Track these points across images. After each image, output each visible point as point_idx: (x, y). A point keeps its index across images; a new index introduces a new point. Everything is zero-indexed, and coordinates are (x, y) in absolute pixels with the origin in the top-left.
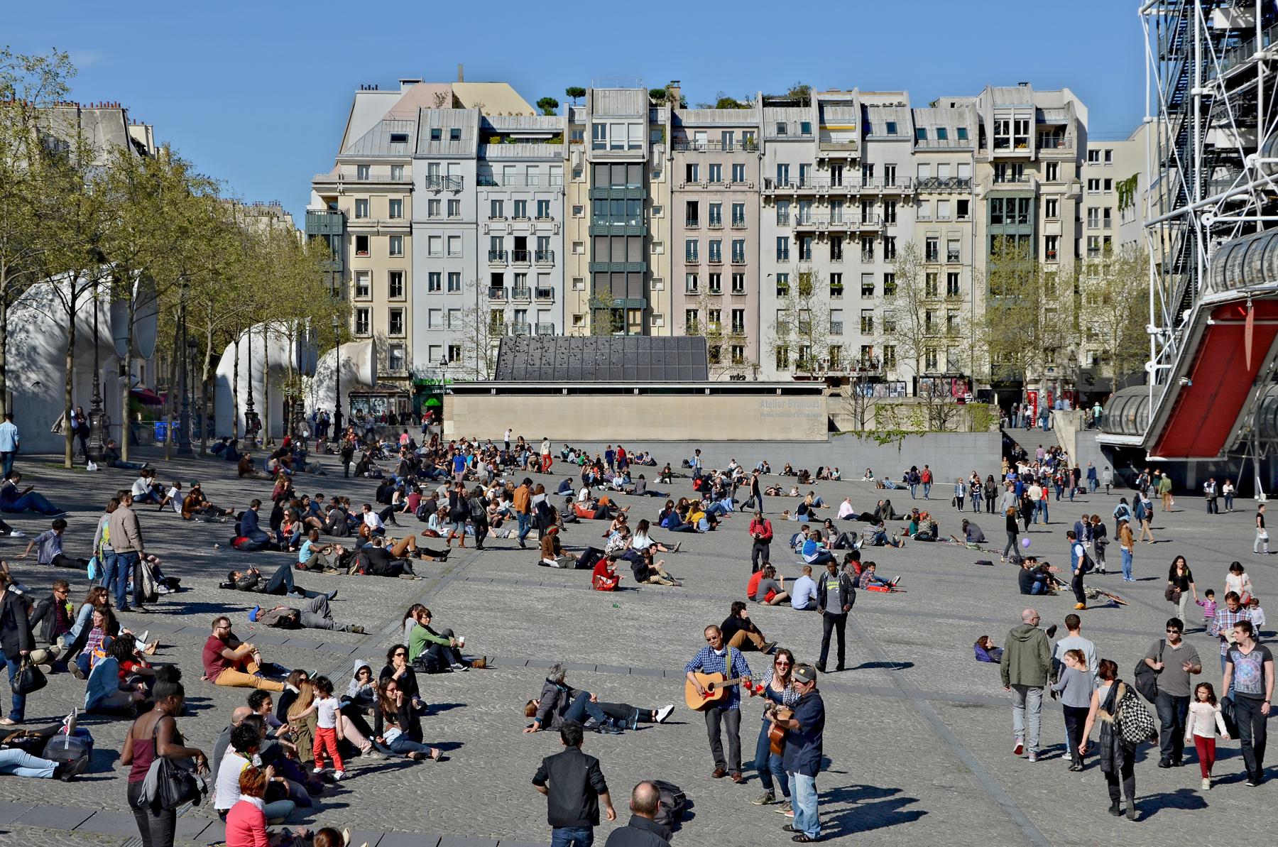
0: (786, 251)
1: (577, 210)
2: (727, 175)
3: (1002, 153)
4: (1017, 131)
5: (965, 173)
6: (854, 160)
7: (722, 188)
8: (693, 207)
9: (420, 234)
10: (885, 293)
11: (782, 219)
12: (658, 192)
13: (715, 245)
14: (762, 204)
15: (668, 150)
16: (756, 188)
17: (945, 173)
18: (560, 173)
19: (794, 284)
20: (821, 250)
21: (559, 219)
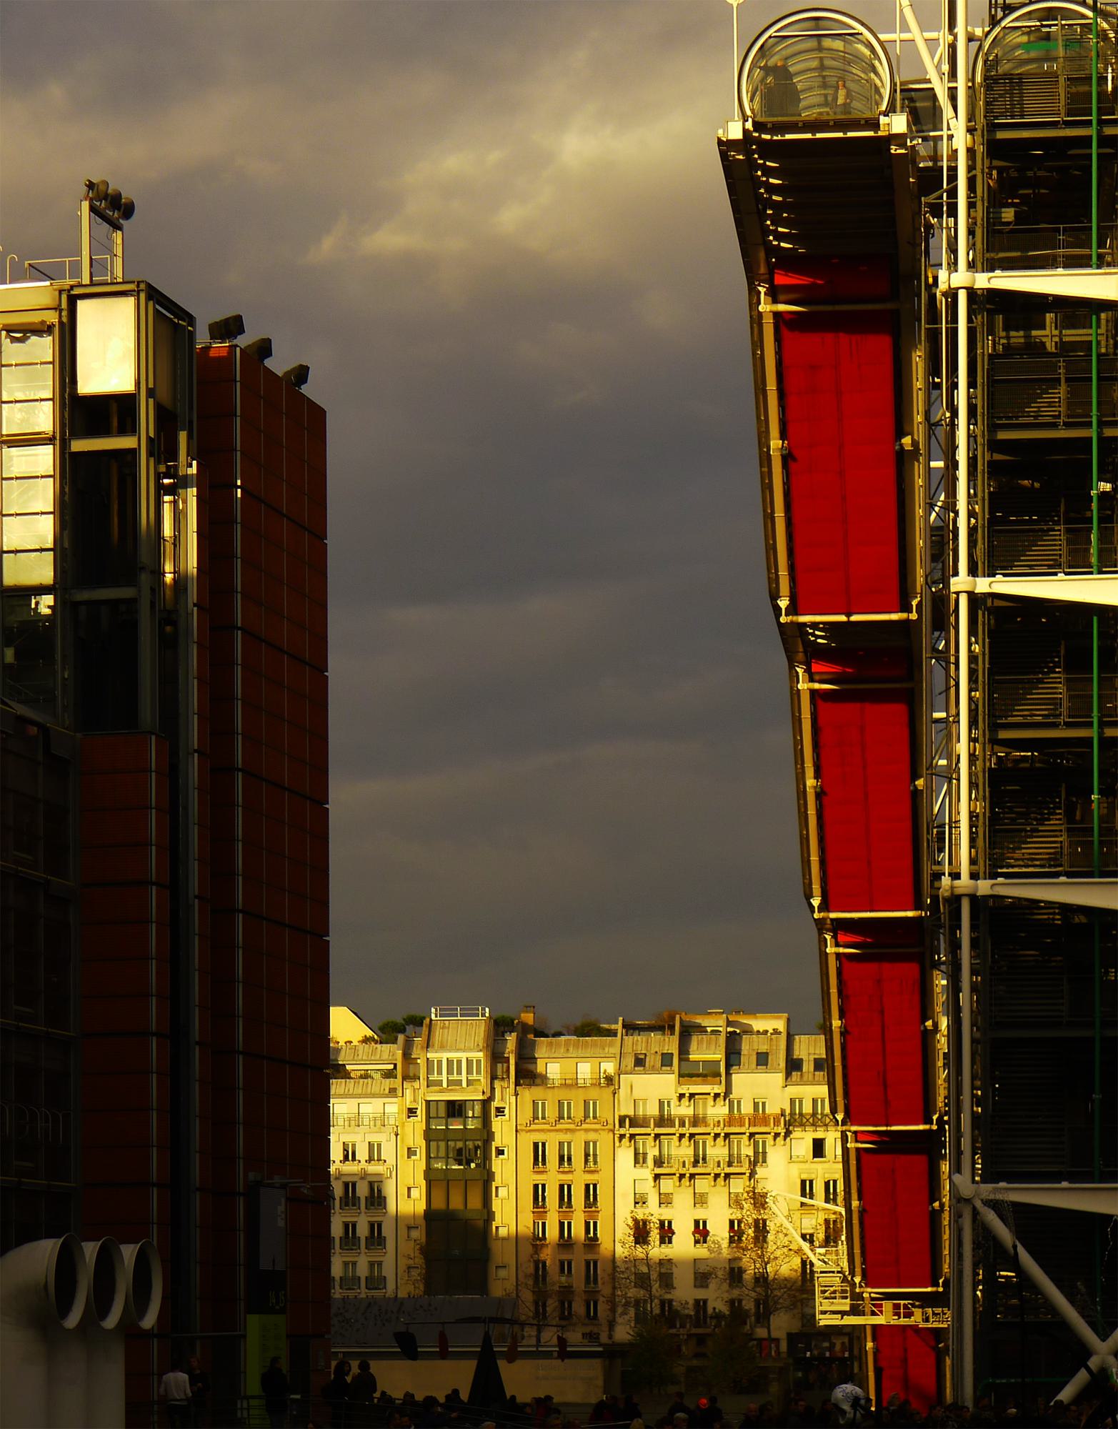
1: (411, 1152)
4: (450, 1072)
6: (717, 1096)
7: (572, 1126)
12: (502, 1130)
13: (564, 1193)
14: (617, 1144)
15: (512, 1086)
18: (393, 1108)
19: (655, 1235)
21: (391, 1162)
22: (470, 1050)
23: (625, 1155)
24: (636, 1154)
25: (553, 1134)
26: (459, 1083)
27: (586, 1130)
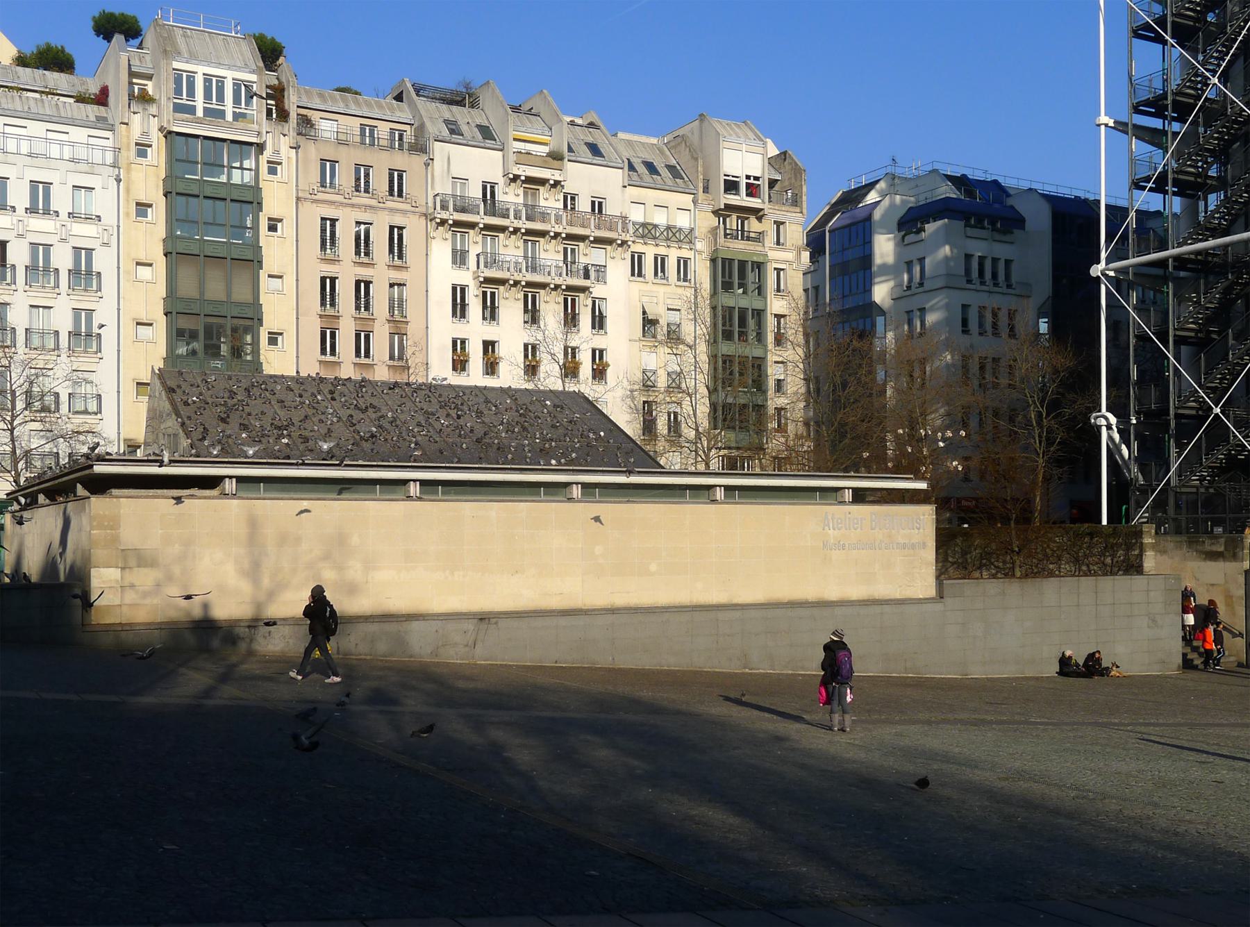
0: (464, 306)
1: (142, 208)
2: (380, 182)
5: (683, 221)
7: (374, 202)
8: (328, 227)
10: (594, 378)
11: (459, 258)
13: (362, 287)
16: (423, 210)
17: (660, 219)
20: (511, 308)
22: (239, 69)
23: (441, 250)
24: (454, 251)
25: (349, 209)
26: (221, 114)
27: (392, 210)
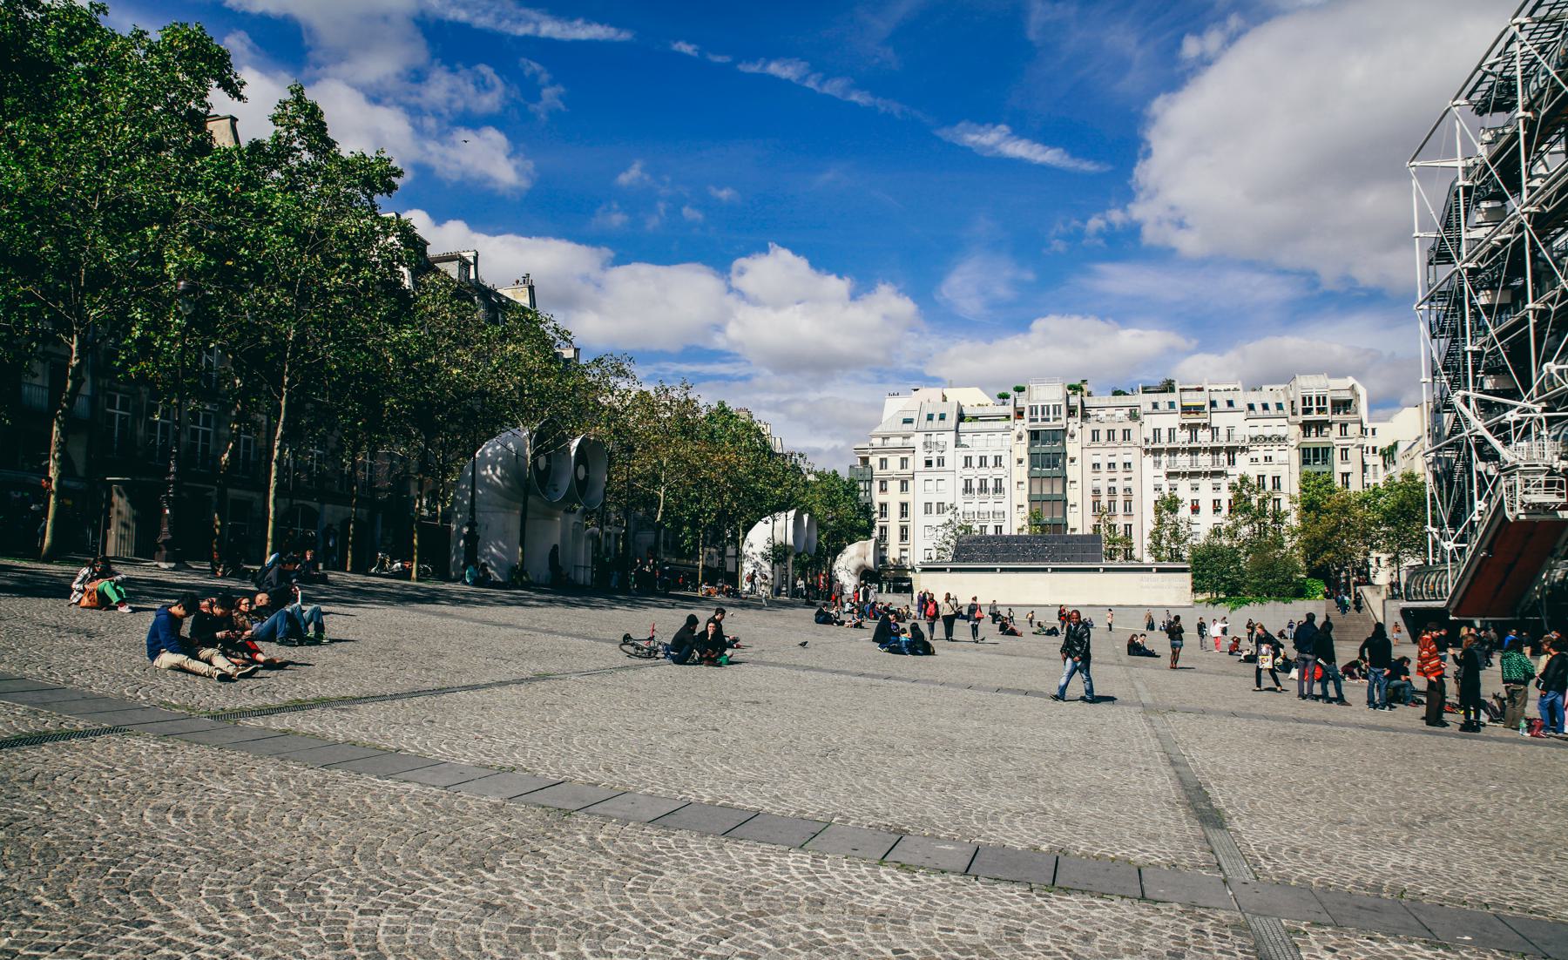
3: (1308, 417)
5: (1282, 432)
9: (919, 478)
13: (1112, 491)
